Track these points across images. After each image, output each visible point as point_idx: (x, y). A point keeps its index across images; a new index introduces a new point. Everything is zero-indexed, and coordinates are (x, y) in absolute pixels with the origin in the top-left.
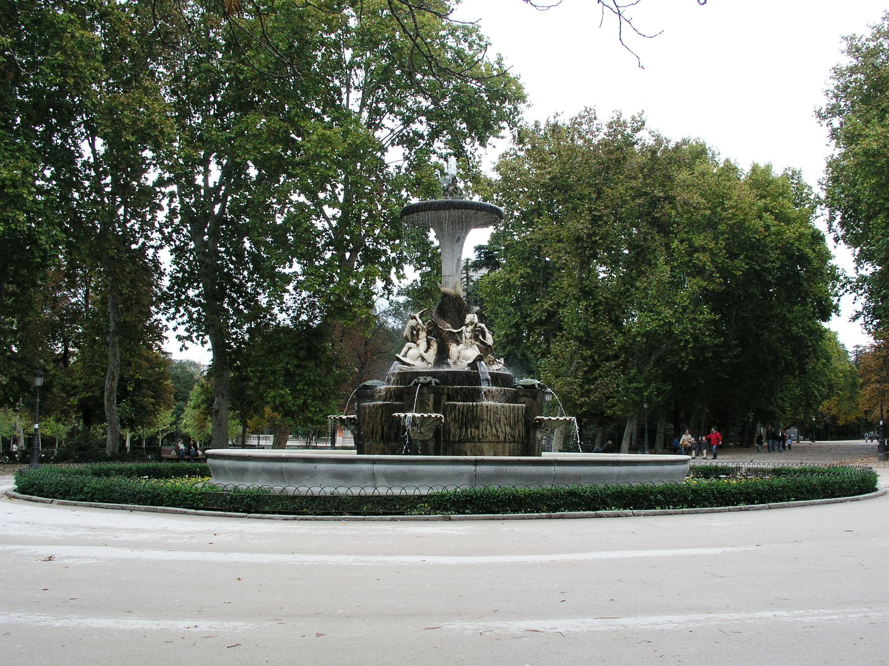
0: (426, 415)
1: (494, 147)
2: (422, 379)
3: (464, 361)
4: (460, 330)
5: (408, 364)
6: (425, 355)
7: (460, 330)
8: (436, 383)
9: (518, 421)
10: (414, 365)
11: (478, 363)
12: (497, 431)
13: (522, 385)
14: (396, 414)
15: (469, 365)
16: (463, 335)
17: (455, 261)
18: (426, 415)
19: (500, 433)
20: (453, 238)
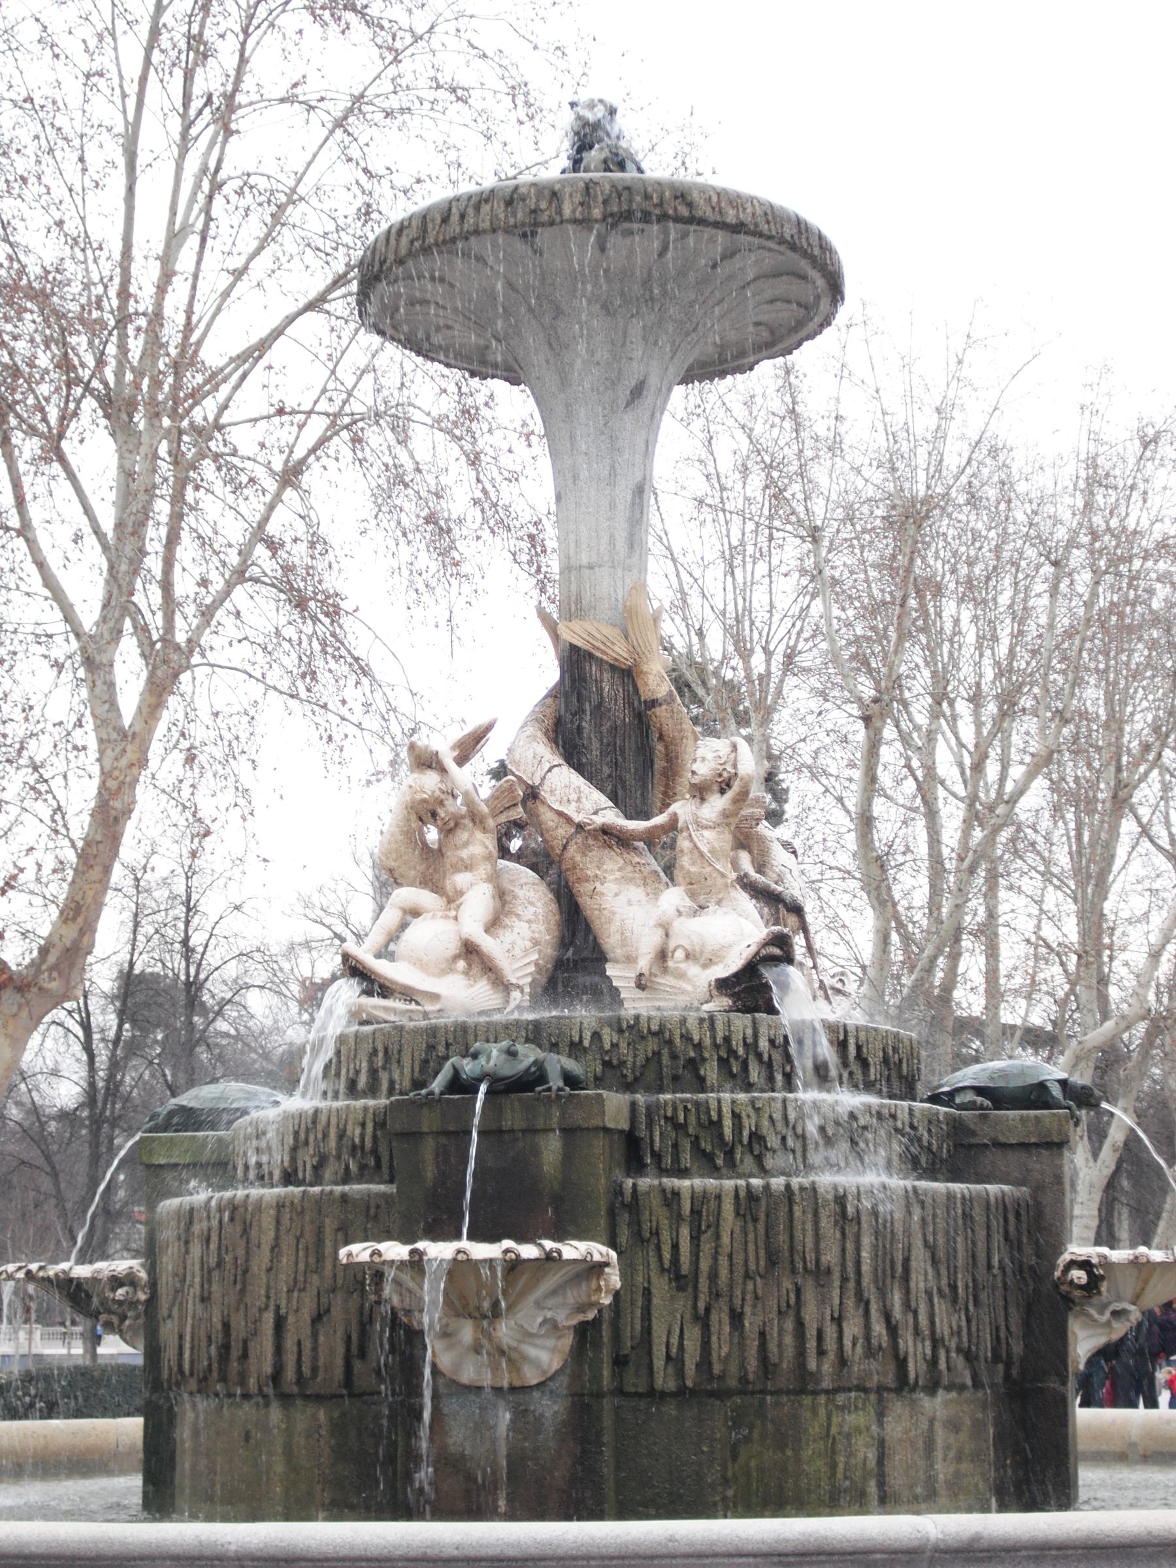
0: (529, 1251)
1: (369, 782)
2: (493, 1057)
3: (693, 970)
4: (659, 820)
5: (408, 994)
6: (487, 943)
7: (659, 820)
8: (571, 1080)
9: (307, 1143)
10: (435, 997)
11: (769, 974)
12: (893, 1330)
13: (979, 1091)
14: (359, 1251)
15: (723, 985)
16: (683, 844)
17: (624, 494)
18: (529, 1251)
19: (907, 1342)
20: (613, 383)
